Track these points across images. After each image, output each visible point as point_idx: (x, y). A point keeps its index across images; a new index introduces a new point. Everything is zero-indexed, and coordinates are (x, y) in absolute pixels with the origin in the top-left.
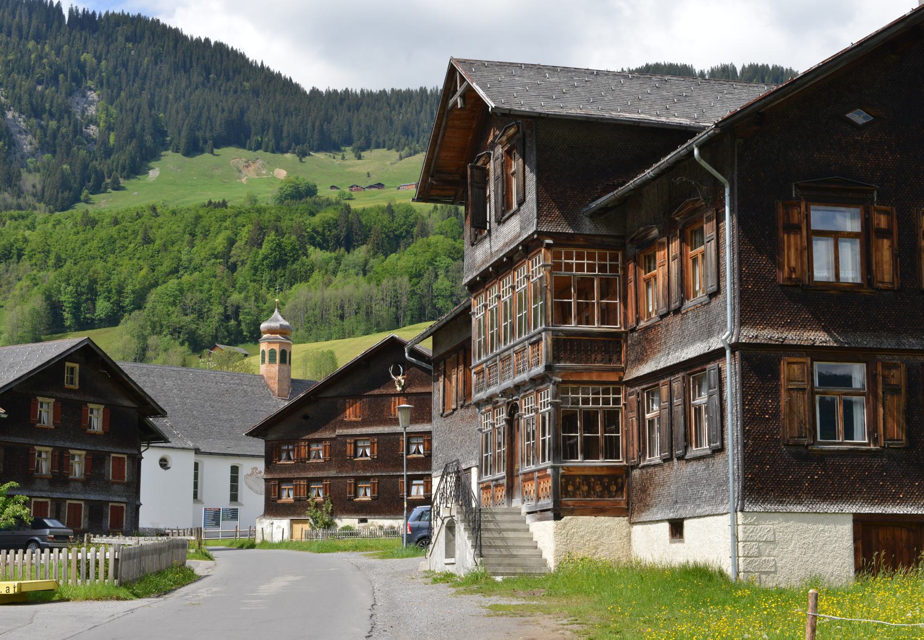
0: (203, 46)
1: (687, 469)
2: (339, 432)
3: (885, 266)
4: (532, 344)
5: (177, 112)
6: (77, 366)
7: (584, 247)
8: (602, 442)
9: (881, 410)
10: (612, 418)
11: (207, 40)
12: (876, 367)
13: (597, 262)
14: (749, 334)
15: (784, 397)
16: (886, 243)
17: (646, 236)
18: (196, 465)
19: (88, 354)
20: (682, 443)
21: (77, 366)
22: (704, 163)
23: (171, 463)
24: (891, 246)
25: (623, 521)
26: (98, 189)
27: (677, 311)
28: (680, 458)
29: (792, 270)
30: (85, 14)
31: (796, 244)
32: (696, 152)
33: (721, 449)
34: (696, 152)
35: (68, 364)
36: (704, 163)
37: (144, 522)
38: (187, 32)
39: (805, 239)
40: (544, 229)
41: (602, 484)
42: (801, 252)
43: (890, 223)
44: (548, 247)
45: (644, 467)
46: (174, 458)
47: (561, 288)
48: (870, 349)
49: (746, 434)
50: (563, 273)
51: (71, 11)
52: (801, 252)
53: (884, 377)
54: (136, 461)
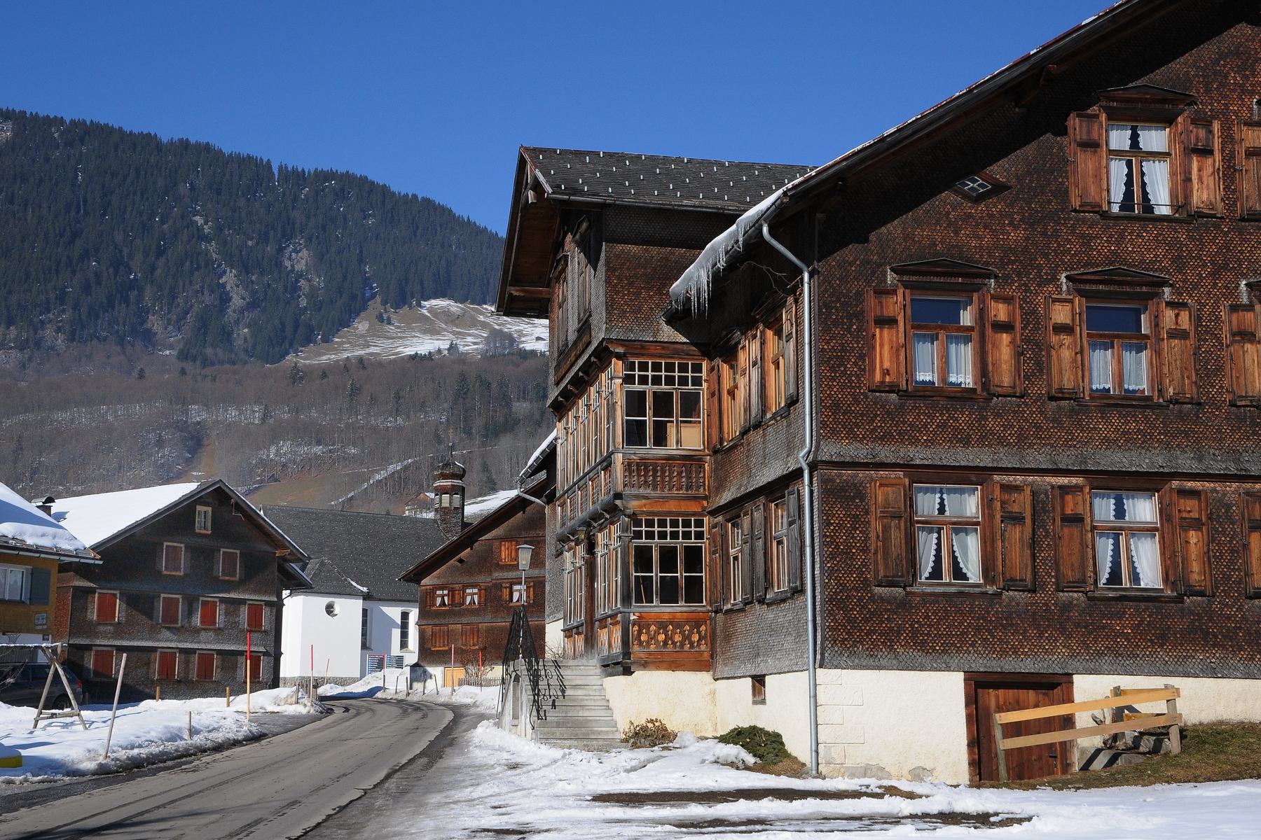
0: (410, 201)
1: (769, 615)
2: (496, 575)
3: (1004, 367)
4: (605, 469)
5: (385, 266)
6: (210, 509)
7: (661, 357)
8: (682, 583)
9: (999, 543)
10: (693, 557)
11: (415, 196)
12: (993, 491)
13: (676, 374)
14: (830, 451)
15: (876, 526)
16: (1005, 338)
17: (729, 340)
18: (365, 612)
19: (218, 496)
20: (762, 587)
21: (210, 509)
22: (774, 243)
23: (337, 609)
24: (1012, 342)
25: (706, 677)
26: (308, 340)
27: (757, 426)
28: (762, 601)
29: (886, 372)
30: (294, 171)
31: (891, 341)
32: (765, 229)
33: (802, 591)
34: (765, 229)
35: (199, 508)
36: (774, 243)
37: (290, 666)
38: (394, 188)
39: (902, 335)
40: (613, 336)
41: (682, 633)
42: (898, 350)
43: (1011, 314)
44: (619, 357)
45: (728, 611)
46: (341, 604)
47: (635, 403)
48: (985, 469)
49: (829, 573)
50: (637, 387)
51: (280, 168)
52: (898, 350)
53: (1003, 502)
54: (278, 607)
